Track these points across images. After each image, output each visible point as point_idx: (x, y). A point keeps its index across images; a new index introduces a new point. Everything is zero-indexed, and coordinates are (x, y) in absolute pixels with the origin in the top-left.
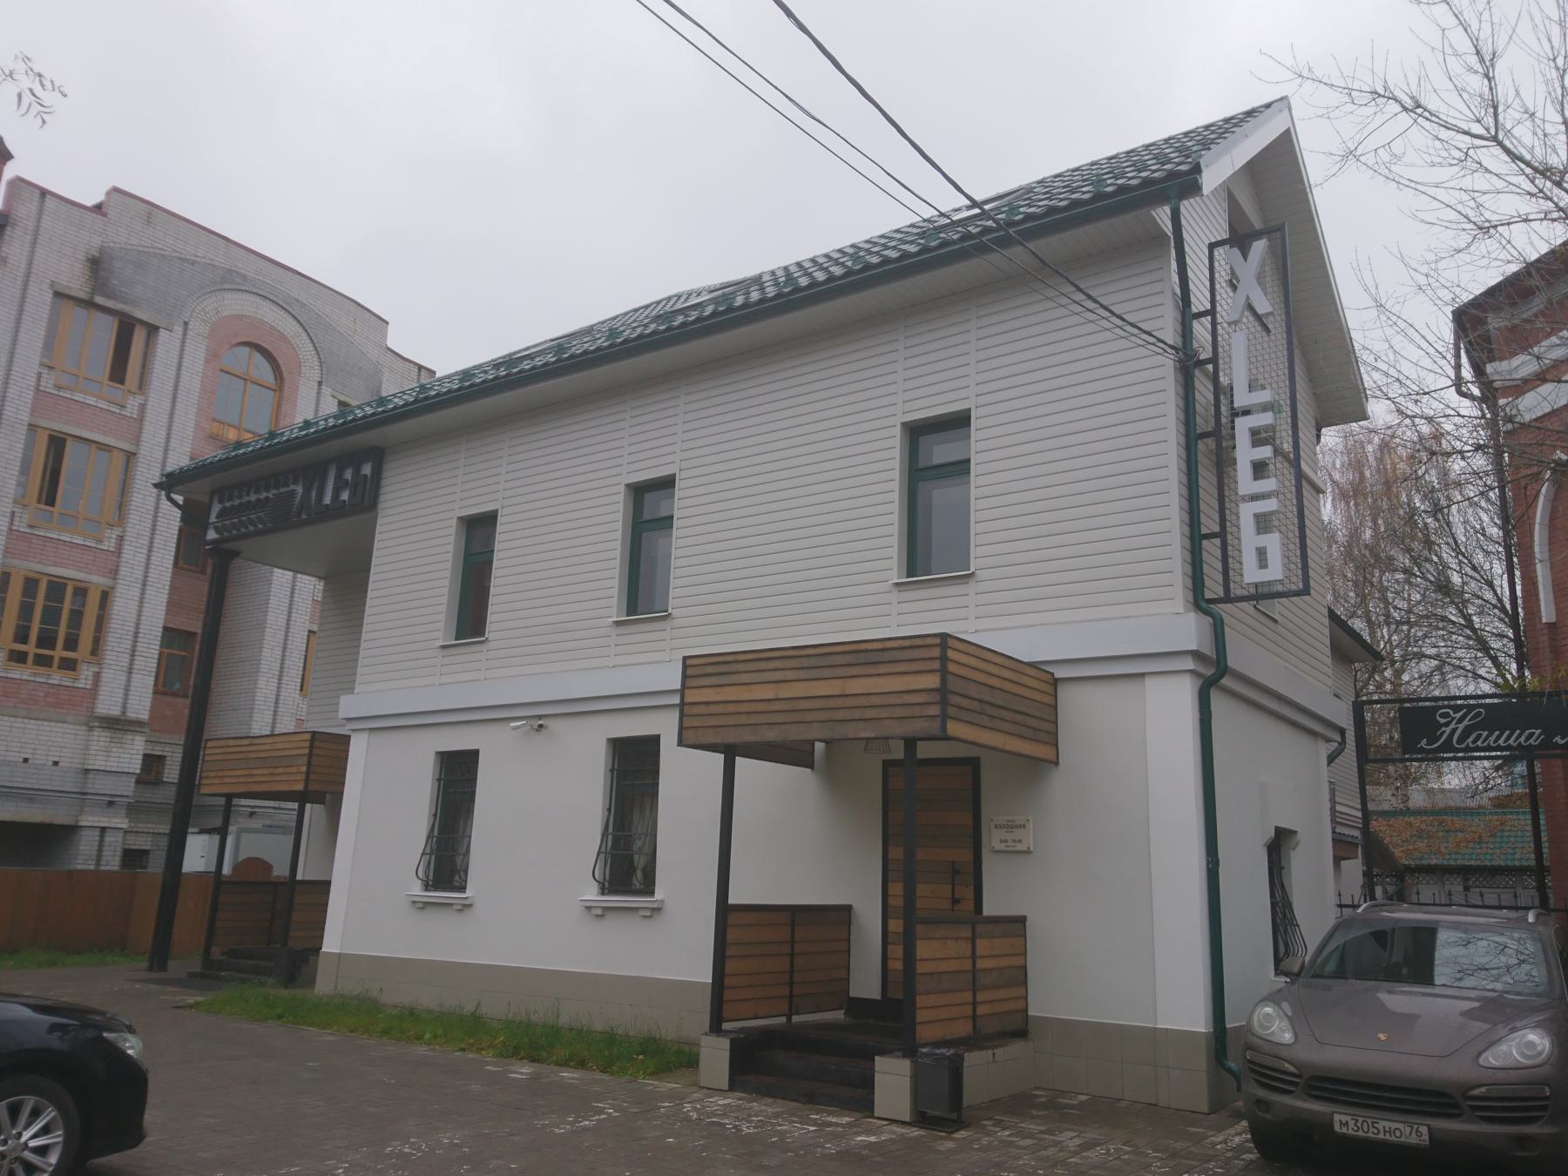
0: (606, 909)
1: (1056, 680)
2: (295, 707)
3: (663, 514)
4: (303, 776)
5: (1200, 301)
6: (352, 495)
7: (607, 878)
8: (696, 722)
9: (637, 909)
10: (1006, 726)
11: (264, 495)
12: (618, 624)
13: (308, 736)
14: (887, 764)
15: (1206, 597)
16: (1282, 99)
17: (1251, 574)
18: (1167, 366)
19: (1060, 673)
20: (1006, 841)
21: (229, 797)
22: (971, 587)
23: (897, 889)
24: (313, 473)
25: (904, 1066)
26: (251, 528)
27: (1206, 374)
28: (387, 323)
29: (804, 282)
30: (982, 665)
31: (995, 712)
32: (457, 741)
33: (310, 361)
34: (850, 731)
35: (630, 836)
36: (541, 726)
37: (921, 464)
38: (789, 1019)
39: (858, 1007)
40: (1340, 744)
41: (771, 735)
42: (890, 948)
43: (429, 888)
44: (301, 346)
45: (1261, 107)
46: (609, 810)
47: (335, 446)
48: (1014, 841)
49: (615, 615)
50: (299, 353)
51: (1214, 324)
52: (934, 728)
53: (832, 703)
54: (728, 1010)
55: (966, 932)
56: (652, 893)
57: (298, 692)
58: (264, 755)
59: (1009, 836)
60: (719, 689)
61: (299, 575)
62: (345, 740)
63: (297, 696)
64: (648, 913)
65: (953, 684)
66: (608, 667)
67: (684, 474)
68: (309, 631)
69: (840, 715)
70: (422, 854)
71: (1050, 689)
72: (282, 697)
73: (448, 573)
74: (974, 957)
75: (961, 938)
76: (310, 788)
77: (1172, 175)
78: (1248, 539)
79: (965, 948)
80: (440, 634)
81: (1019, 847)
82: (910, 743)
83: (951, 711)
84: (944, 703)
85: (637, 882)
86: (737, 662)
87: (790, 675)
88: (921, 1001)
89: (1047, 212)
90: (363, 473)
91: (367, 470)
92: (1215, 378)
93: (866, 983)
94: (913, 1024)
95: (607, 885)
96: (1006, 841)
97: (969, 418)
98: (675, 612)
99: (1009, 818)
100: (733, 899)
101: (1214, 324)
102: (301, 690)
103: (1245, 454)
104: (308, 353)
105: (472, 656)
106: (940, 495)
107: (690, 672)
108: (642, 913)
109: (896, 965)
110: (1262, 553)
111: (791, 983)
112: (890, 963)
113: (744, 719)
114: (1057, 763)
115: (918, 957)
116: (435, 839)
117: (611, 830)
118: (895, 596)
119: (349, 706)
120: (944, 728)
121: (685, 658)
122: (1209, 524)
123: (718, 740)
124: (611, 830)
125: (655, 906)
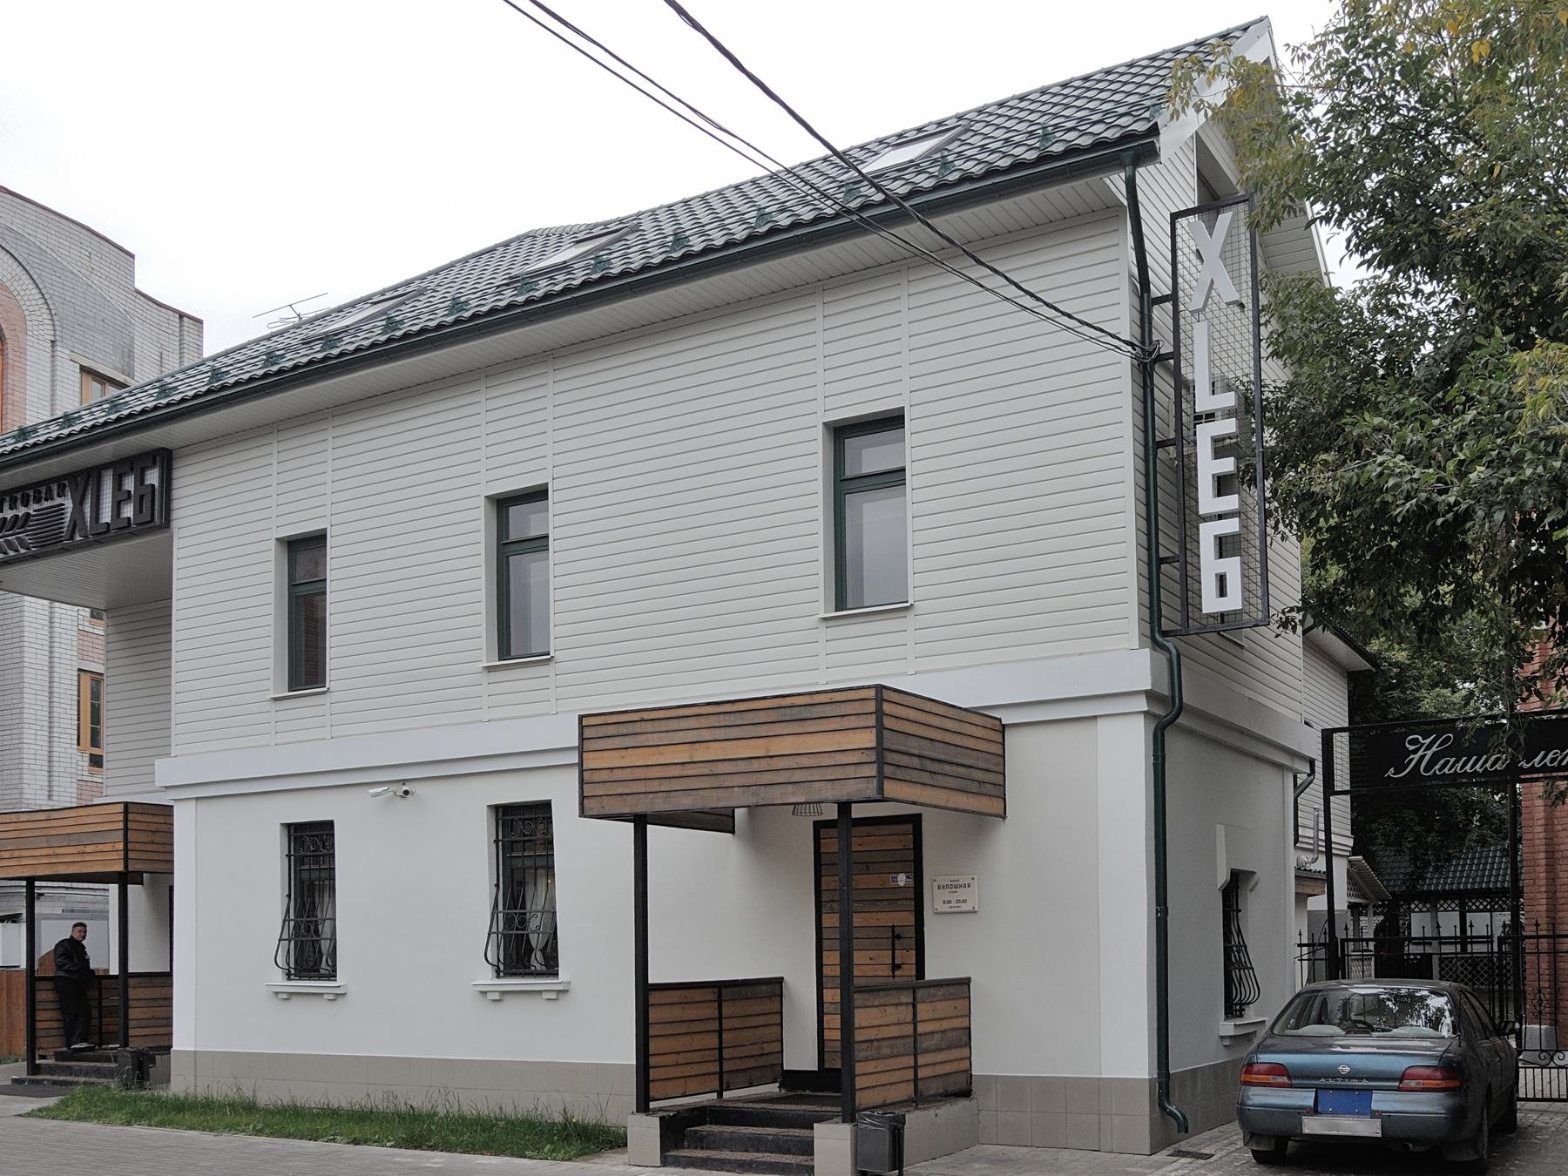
0: (503, 993)
1: (1004, 726)
2: (74, 766)
3: (533, 533)
4: (122, 855)
5: (1160, 286)
6: (139, 510)
7: (502, 960)
8: (599, 790)
9: (540, 992)
10: (950, 782)
11: (21, 511)
12: (489, 669)
13: (121, 808)
14: (819, 826)
15: (1164, 628)
16: (1261, 20)
17: (1211, 603)
18: (1122, 366)
19: (1007, 718)
20: (949, 902)
21: (31, 881)
22: (909, 621)
23: (832, 958)
24: (84, 481)
25: (845, 1130)
26: (11, 553)
27: (1167, 368)
28: (132, 256)
29: (697, 244)
30: (922, 717)
31: (936, 767)
32: (308, 811)
33: (38, 313)
34: (776, 795)
35: (525, 914)
36: (406, 792)
37: (849, 473)
38: (720, 1095)
39: (794, 1081)
40: (1309, 775)
41: (686, 803)
42: (826, 1018)
43: (292, 977)
44: (22, 293)
45: (1237, 29)
46: (497, 885)
47: (108, 450)
48: (958, 901)
49: (484, 659)
50: (22, 303)
51: (1176, 312)
52: (871, 790)
53: (755, 765)
54: (654, 1090)
55: (906, 998)
56: (556, 974)
57: (76, 747)
58: (69, 830)
59: (953, 897)
60: (624, 752)
61: (57, 604)
62: (167, 811)
63: (75, 751)
64: (553, 996)
65: (891, 741)
66: (481, 721)
67: (558, 484)
68: (79, 670)
69: (766, 778)
70: (280, 941)
71: (998, 737)
72: (55, 754)
73: (271, 609)
74: (915, 1022)
75: (901, 1004)
76: (130, 869)
77: (1129, 137)
78: (1210, 564)
79: (906, 1014)
80: (270, 684)
81: (964, 907)
82: (844, 807)
83: (888, 770)
84: (881, 762)
85: (537, 961)
86: (642, 720)
87: (706, 735)
88: (859, 1068)
89: (986, 172)
90: (148, 482)
91: (153, 477)
92: (1176, 373)
93: (801, 1054)
94: (853, 1090)
95: (502, 967)
96: (949, 902)
97: (903, 417)
98: (558, 655)
99: (953, 878)
100: (654, 978)
101: (1176, 312)
102: (78, 744)
103: (1208, 467)
104: (34, 303)
105: (308, 707)
106: (870, 511)
107: (587, 733)
108: (545, 996)
109: (834, 1035)
110: (1222, 579)
111: (721, 1060)
112: (827, 1033)
113: (655, 786)
114: (1004, 817)
115: (856, 1025)
116: (292, 923)
117: (501, 908)
118: (824, 632)
119: (167, 772)
120: (881, 789)
121: (581, 718)
122: (1167, 547)
123: (627, 810)
124: (501, 908)
125: (560, 988)
